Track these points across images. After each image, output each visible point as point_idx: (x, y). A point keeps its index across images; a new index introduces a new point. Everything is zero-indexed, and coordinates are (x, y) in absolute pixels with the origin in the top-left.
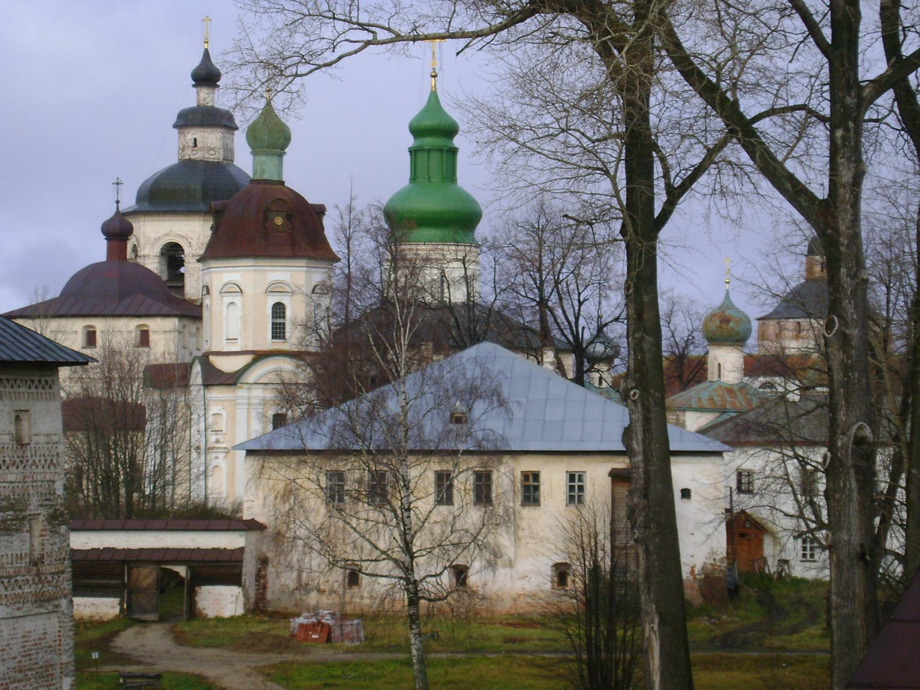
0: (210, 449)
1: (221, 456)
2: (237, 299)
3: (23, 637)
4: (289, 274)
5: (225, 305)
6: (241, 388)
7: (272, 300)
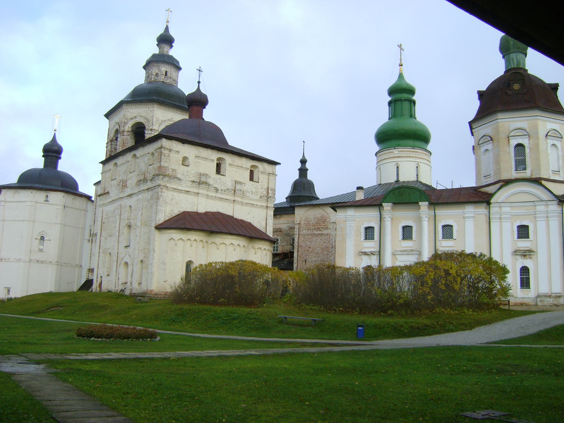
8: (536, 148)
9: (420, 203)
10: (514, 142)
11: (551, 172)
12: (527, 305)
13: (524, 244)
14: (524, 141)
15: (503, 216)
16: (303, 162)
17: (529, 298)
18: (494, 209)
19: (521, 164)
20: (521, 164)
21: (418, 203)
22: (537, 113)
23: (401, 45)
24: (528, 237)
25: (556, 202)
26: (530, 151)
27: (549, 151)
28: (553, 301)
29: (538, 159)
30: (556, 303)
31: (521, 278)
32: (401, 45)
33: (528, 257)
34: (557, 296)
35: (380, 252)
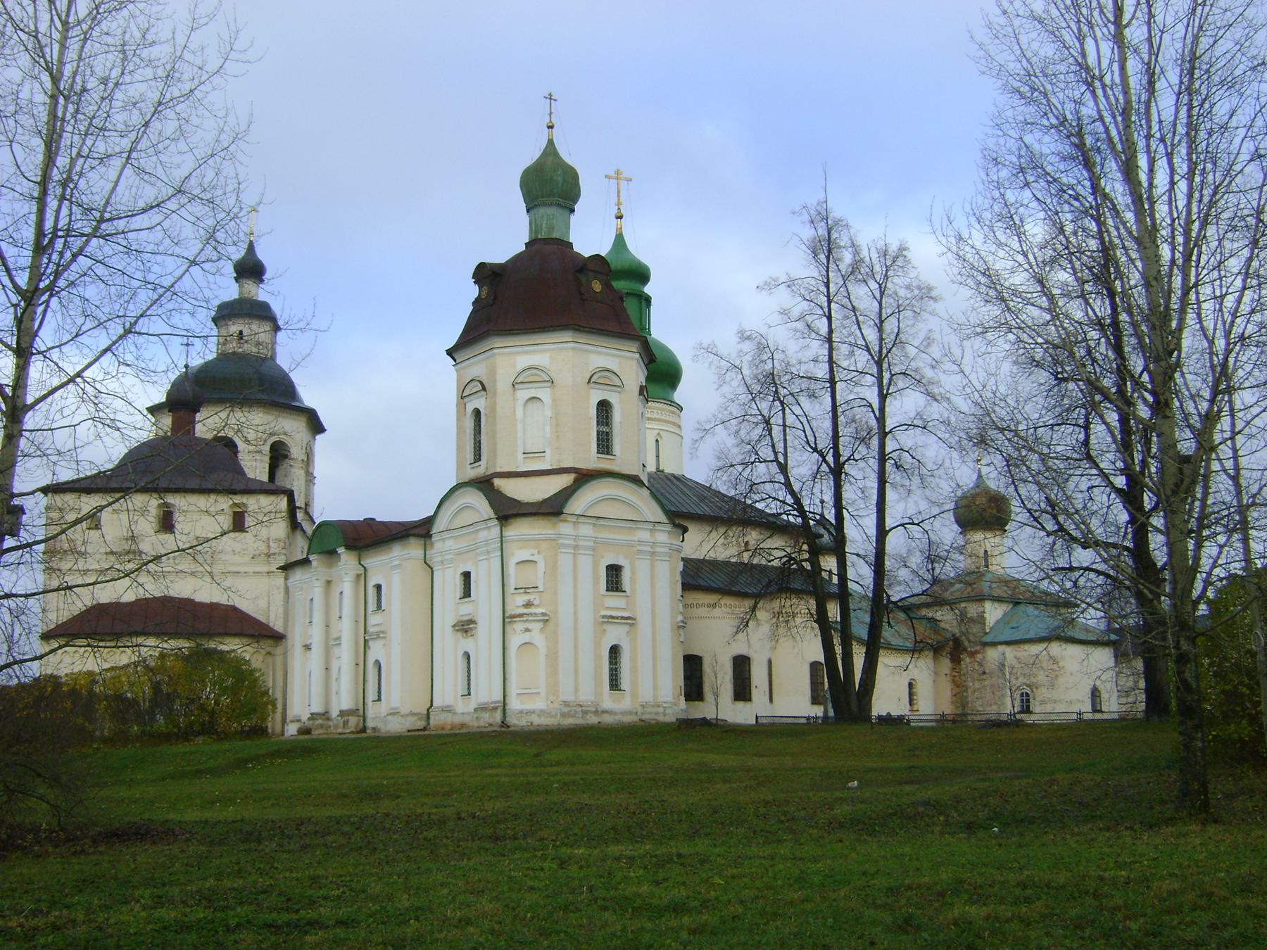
0: (513, 617)
1: (536, 627)
2: (545, 394)
3: (741, 665)
4: (617, 360)
5: (520, 403)
6: (565, 521)
7: (596, 396)
8: (493, 408)
22: (497, 342)
23: (618, 172)
25: (495, 522)
27: (519, 413)
32: (618, 172)
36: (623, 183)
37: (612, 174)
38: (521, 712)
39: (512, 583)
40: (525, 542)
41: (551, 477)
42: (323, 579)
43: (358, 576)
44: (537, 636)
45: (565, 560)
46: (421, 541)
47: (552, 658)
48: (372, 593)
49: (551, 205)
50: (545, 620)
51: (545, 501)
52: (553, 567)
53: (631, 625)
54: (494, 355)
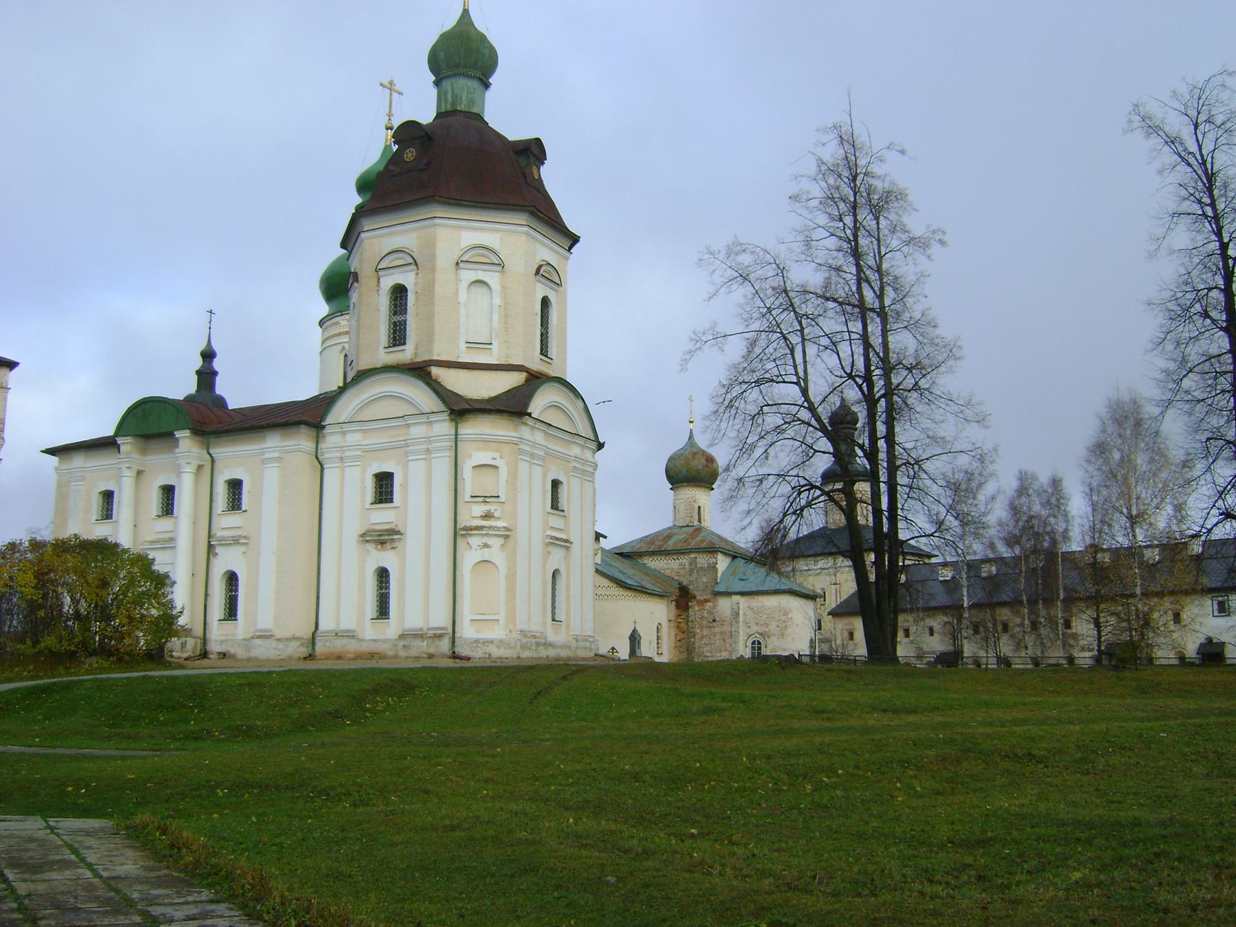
1: (496, 542)
2: (493, 278)
6: (526, 424)
7: (541, 290)
8: (429, 289)
9: (178, 434)
10: (388, 282)
11: (463, 346)
12: (382, 657)
13: (383, 516)
14: (407, 278)
15: (348, 454)
16: (208, 355)
17: (385, 641)
18: (331, 439)
19: (398, 336)
20: (398, 336)
21: (170, 435)
22: (439, 211)
23: (391, 83)
24: (392, 501)
25: (445, 416)
26: (417, 299)
27: (463, 296)
28: (428, 646)
29: (430, 317)
30: (432, 650)
31: (236, 590)
32: (391, 83)
33: (388, 546)
34: (435, 636)
35: (211, 547)
36: (395, 95)
37: (386, 83)
38: (477, 641)
39: (467, 490)
40: (486, 442)
41: (499, 373)
42: (136, 468)
43: (200, 467)
44: (495, 552)
45: (523, 467)
46: (313, 432)
47: (511, 579)
48: (221, 491)
49: (474, 77)
50: (506, 535)
51: (496, 397)
52: (513, 474)
53: (567, 548)
54: (435, 225)
